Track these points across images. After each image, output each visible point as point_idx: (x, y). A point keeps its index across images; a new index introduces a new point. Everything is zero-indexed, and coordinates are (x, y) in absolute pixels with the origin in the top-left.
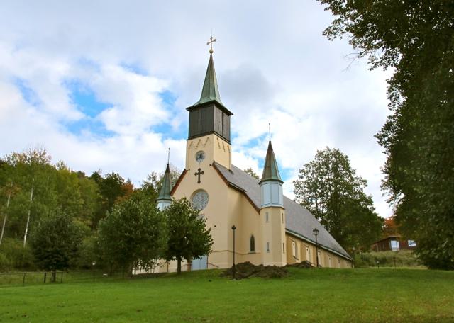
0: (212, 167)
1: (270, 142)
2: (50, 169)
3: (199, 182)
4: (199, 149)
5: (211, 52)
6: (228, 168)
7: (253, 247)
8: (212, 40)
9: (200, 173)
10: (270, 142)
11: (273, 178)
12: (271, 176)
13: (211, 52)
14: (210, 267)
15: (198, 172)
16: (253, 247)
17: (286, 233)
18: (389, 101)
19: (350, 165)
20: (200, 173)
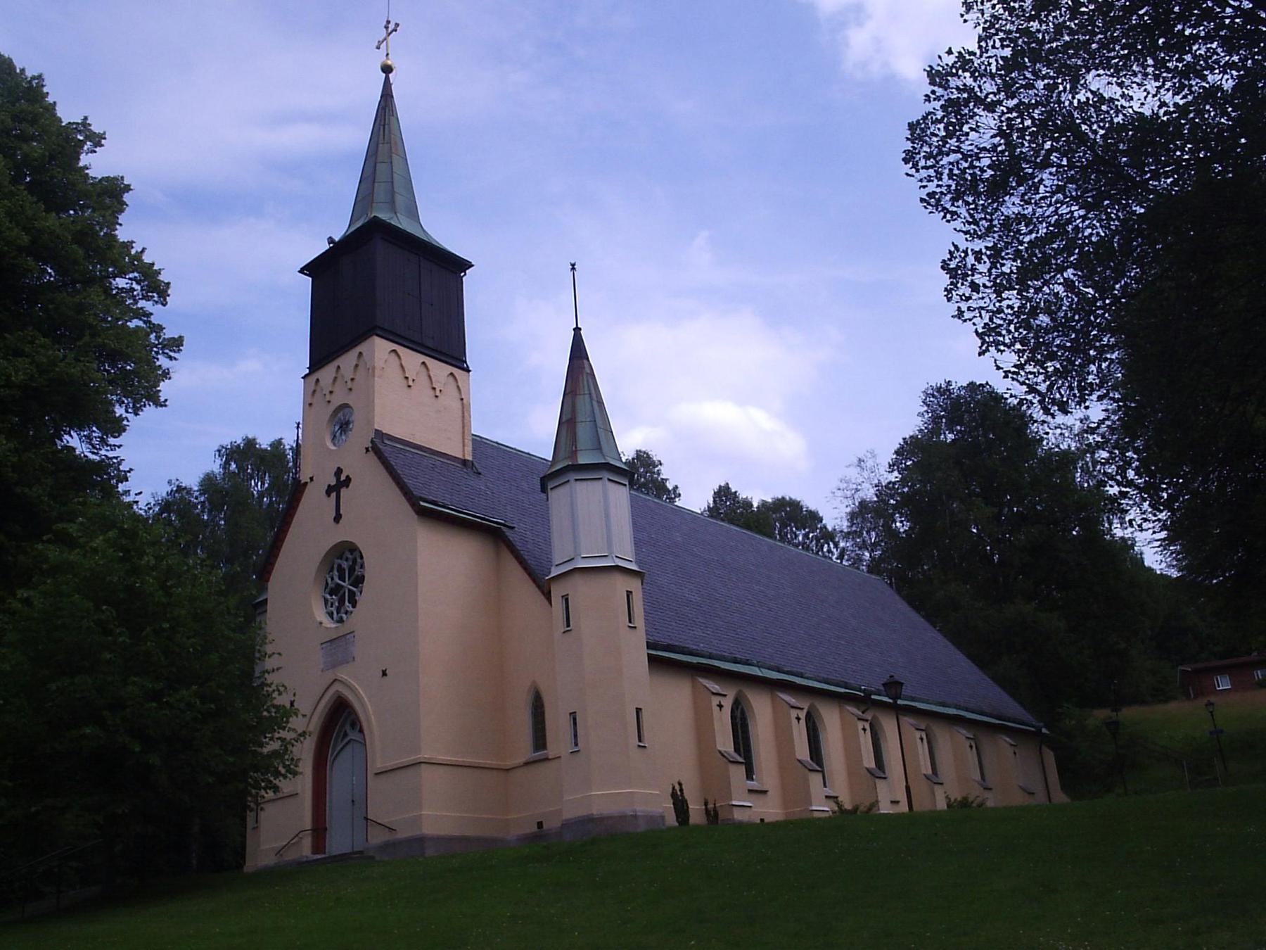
0: (371, 453)
1: (577, 330)
2: (54, 115)
3: (338, 518)
4: (338, 400)
5: (387, 69)
6: (460, 456)
7: (540, 740)
8: (391, 28)
9: (340, 483)
10: (577, 330)
11: (583, 459)
12: (574, 453)
13: (387, 69)
14: (377, 838)
15: (333, 482)
16: (540, 740)
17: (652, 659)
18: (909, 146)
19: (264, 442)
20: (340, 483)
